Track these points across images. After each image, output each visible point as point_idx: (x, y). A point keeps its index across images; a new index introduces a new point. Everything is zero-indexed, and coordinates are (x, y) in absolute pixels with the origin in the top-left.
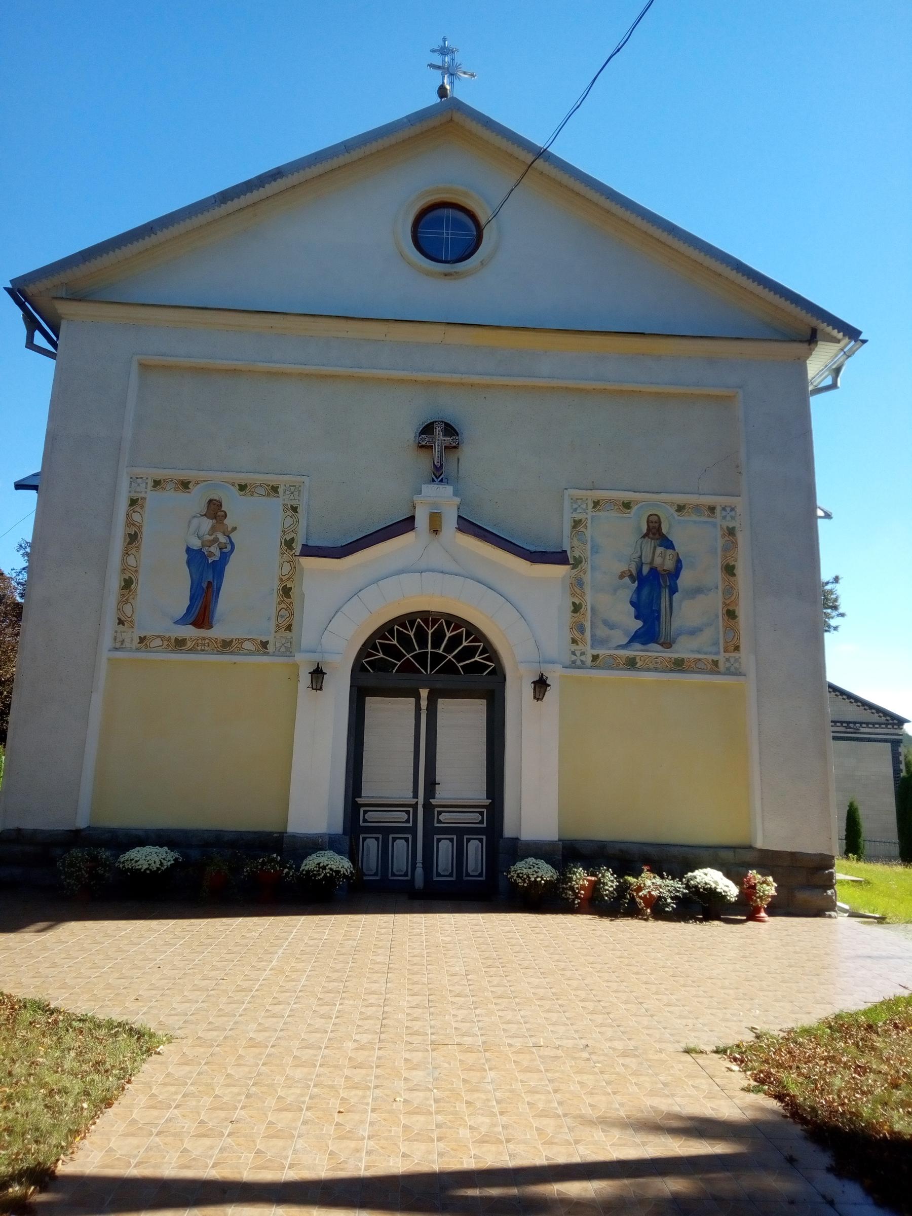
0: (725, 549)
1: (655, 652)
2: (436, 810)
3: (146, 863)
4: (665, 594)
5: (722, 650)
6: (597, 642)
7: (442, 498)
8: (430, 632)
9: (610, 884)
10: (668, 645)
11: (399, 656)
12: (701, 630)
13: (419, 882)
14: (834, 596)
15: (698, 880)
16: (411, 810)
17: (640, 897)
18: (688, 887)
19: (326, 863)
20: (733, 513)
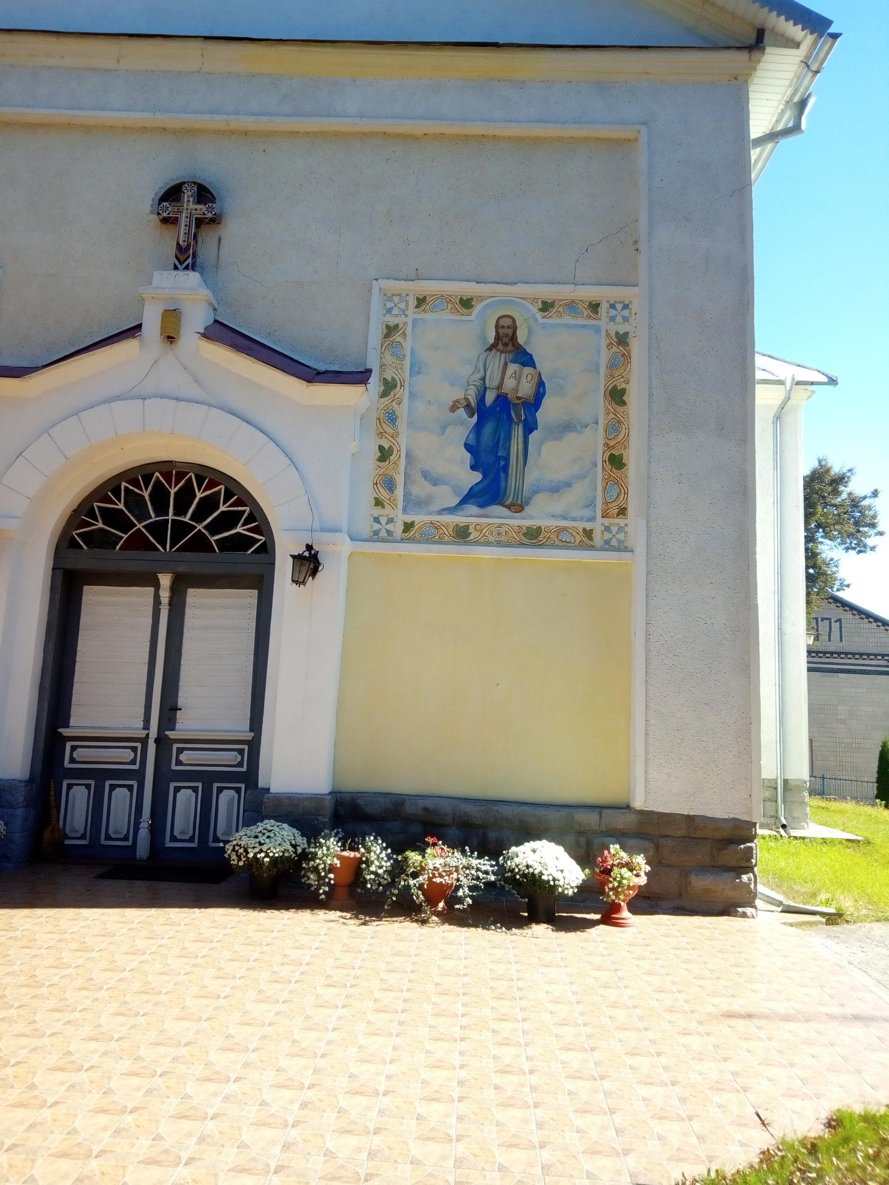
0: (612, 366)
1: (498, 517)
2: (175, 746)
4: (518, 432)
5: (599, 514)
6: (411, 502)
7: (190, 291)
8: (173, 491)
10: (518, 507)
11: (126, 525)
13: (143, 850)
14: (872, 513)
16: (139, 745)
20: (626, 313)
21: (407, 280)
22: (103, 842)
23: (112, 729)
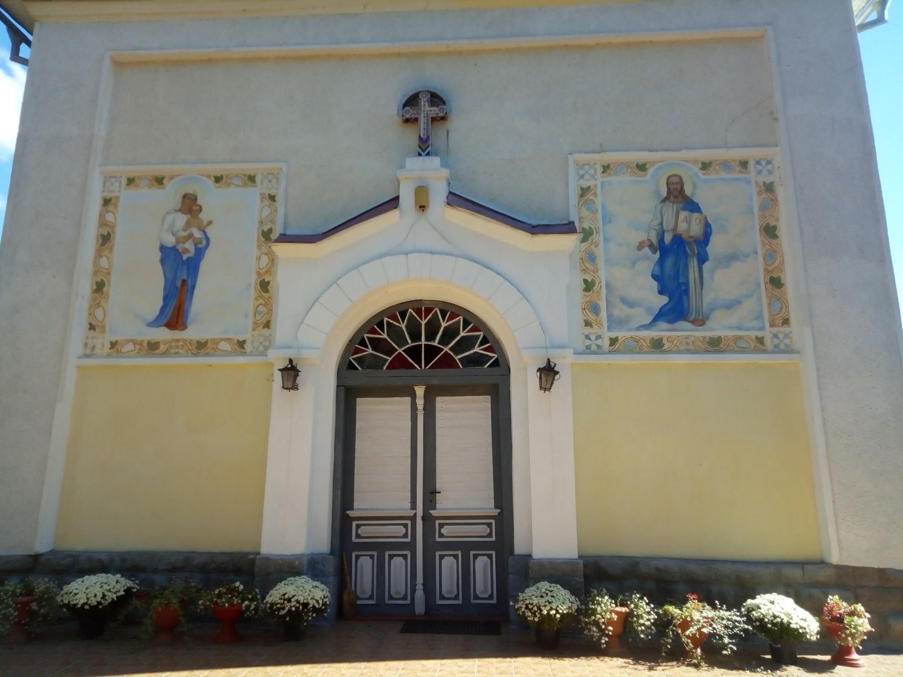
0: (763, 208)
1: (684, 331)
2: (437, 522)
3: (85, 597)
4: (693, 264)
5: (767, 324)
6: (613, 323)
7: (432, 171)
8: (423, 323)
9: (646, 616)
10: (700, 322)
11: (390, 351)
12: (739, 302)
13: (420, 608)
15: (762, 611)
16: (409, 522)
17: (688, 637)
18: (749, 621)
19: (293, 593)
20: (770, 167)
21: (594, 153)
22: (388, 602)
23: (383, 510)
